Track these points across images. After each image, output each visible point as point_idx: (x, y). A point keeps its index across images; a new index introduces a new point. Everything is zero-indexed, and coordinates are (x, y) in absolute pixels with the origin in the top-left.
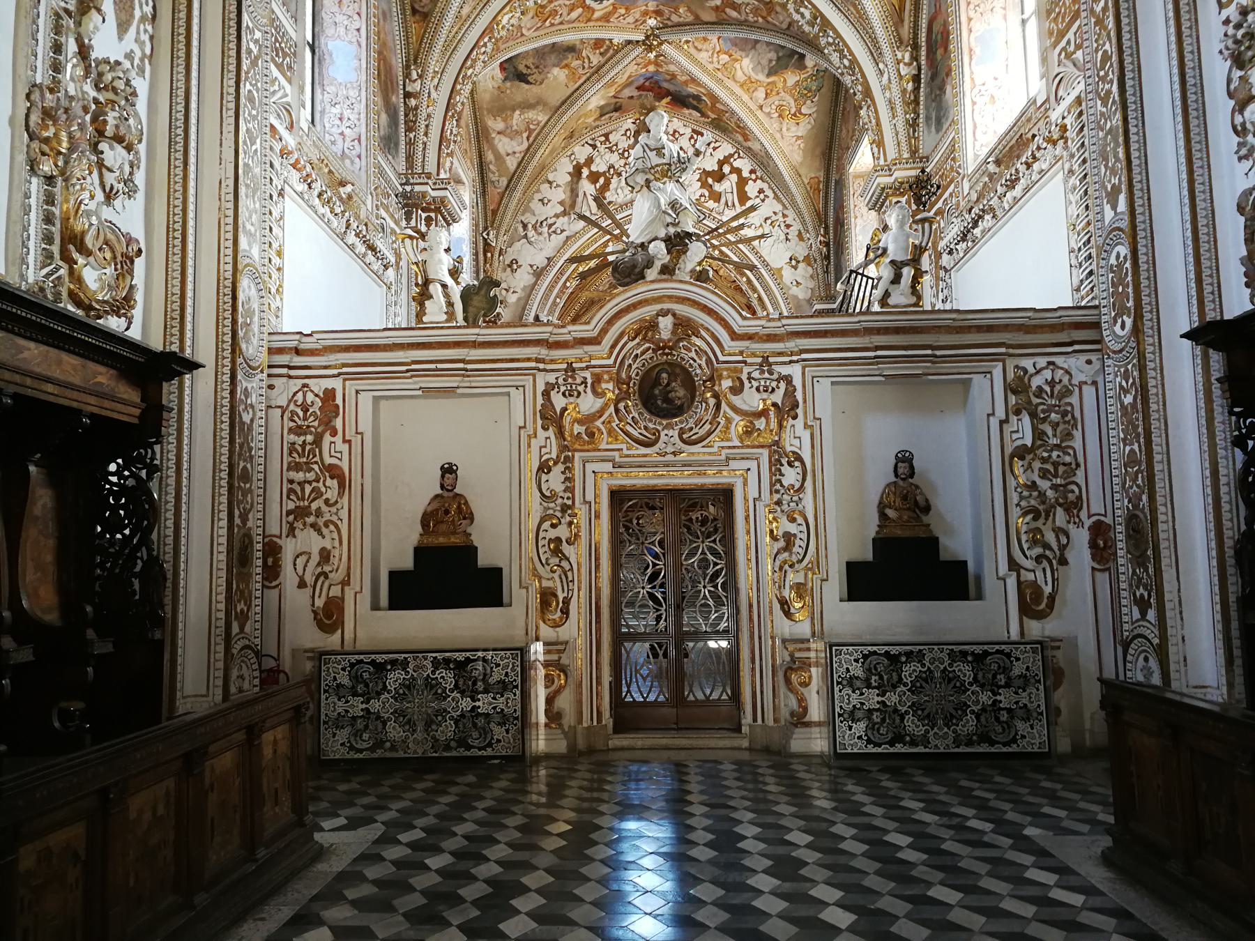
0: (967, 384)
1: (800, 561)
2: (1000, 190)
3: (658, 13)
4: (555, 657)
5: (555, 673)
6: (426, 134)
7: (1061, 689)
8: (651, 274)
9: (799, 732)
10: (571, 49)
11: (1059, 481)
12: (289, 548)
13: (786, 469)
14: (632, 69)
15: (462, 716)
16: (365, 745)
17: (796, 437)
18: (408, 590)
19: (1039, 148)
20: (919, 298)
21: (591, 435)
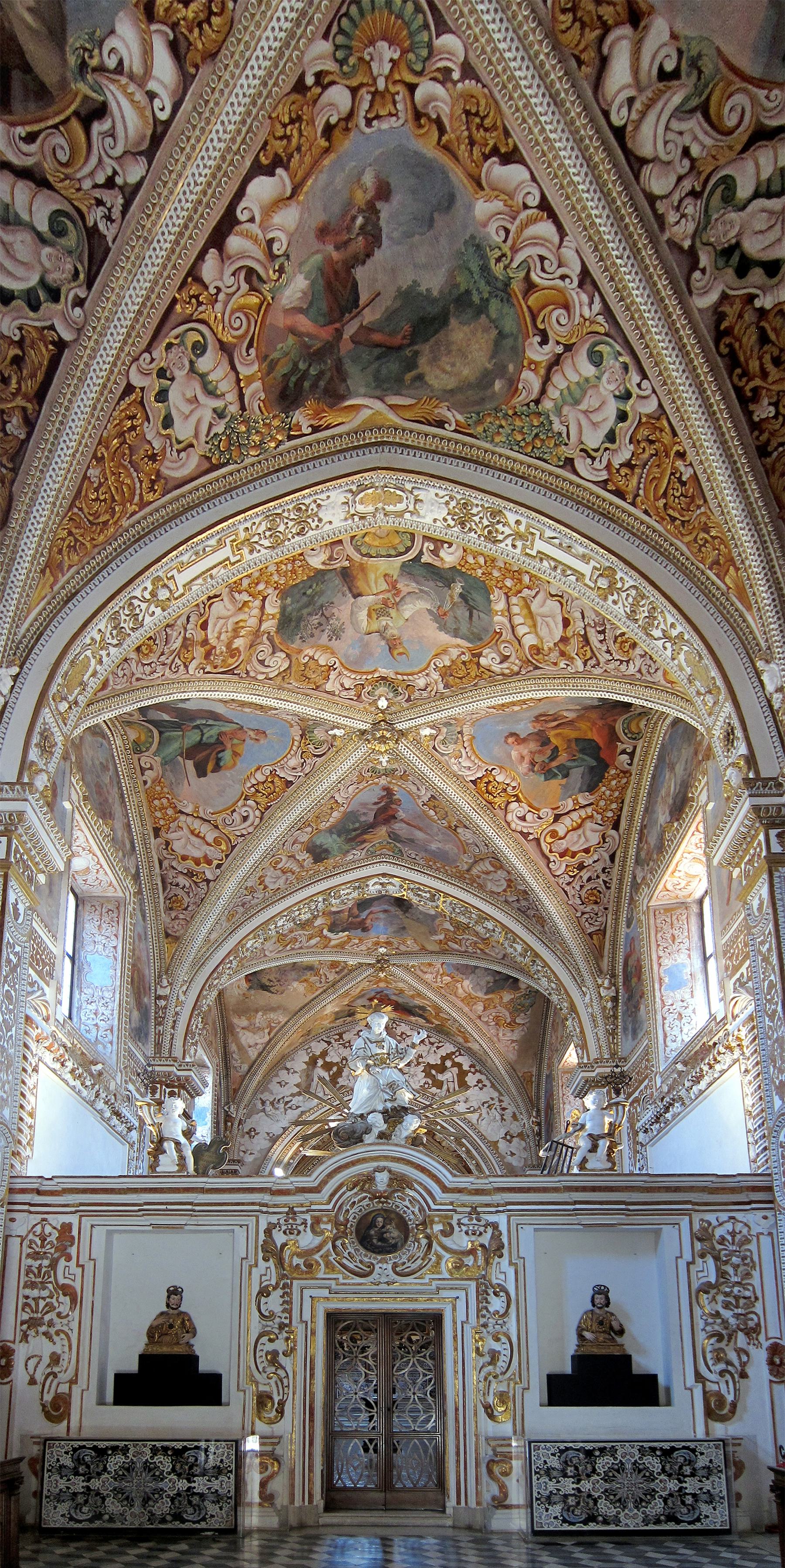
0: (658, 1233)
1: (504, 1373)
2: (687, 1084)
3: (388, 944)
4: (269, 1448)
5: (269, 1462)
6: (173, 1027)
7: (741, 1479)
8: (369, 1139)
9: (500, 1513)
10: (310, 968)
11: (740, 1311)
12: (21, 1352)
13: (492, 1298)
14: (365, 984)
15: (179, 1494)
16: (84, 1517)
17: (502, 1272)
18: (130, 1390)
19: (719, 1053)
20: (614, 1164)
21: (309, 1266)
